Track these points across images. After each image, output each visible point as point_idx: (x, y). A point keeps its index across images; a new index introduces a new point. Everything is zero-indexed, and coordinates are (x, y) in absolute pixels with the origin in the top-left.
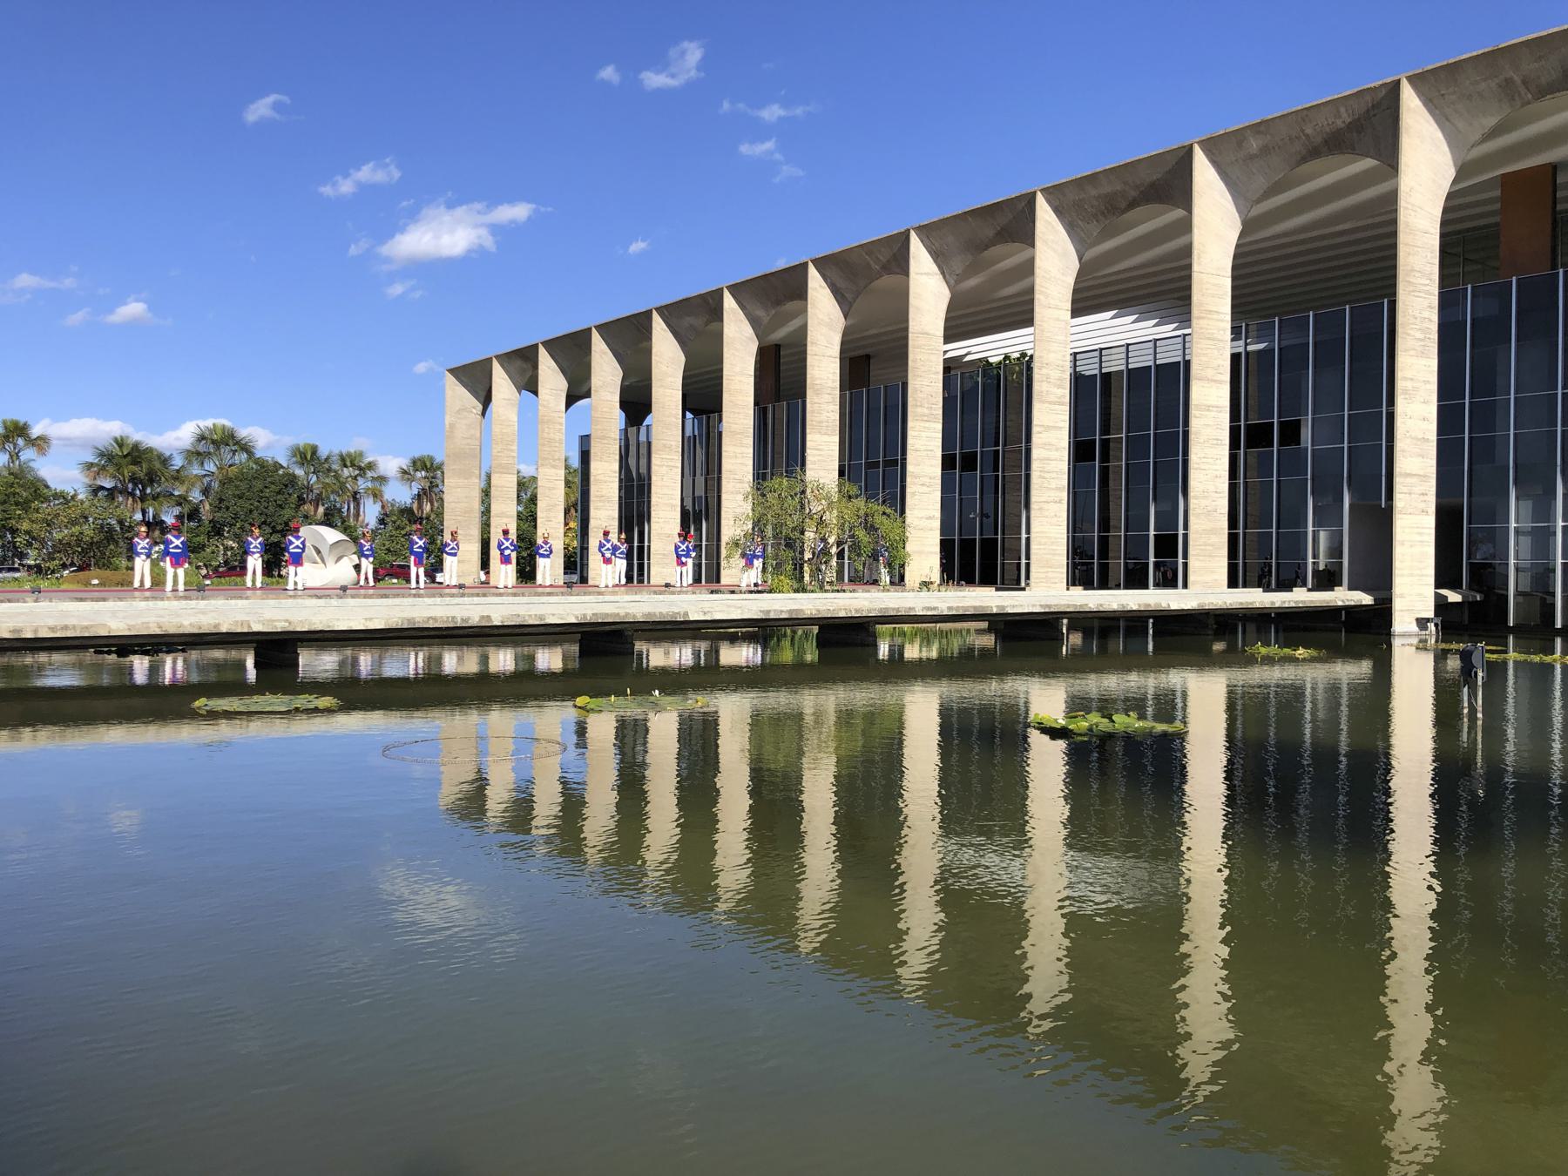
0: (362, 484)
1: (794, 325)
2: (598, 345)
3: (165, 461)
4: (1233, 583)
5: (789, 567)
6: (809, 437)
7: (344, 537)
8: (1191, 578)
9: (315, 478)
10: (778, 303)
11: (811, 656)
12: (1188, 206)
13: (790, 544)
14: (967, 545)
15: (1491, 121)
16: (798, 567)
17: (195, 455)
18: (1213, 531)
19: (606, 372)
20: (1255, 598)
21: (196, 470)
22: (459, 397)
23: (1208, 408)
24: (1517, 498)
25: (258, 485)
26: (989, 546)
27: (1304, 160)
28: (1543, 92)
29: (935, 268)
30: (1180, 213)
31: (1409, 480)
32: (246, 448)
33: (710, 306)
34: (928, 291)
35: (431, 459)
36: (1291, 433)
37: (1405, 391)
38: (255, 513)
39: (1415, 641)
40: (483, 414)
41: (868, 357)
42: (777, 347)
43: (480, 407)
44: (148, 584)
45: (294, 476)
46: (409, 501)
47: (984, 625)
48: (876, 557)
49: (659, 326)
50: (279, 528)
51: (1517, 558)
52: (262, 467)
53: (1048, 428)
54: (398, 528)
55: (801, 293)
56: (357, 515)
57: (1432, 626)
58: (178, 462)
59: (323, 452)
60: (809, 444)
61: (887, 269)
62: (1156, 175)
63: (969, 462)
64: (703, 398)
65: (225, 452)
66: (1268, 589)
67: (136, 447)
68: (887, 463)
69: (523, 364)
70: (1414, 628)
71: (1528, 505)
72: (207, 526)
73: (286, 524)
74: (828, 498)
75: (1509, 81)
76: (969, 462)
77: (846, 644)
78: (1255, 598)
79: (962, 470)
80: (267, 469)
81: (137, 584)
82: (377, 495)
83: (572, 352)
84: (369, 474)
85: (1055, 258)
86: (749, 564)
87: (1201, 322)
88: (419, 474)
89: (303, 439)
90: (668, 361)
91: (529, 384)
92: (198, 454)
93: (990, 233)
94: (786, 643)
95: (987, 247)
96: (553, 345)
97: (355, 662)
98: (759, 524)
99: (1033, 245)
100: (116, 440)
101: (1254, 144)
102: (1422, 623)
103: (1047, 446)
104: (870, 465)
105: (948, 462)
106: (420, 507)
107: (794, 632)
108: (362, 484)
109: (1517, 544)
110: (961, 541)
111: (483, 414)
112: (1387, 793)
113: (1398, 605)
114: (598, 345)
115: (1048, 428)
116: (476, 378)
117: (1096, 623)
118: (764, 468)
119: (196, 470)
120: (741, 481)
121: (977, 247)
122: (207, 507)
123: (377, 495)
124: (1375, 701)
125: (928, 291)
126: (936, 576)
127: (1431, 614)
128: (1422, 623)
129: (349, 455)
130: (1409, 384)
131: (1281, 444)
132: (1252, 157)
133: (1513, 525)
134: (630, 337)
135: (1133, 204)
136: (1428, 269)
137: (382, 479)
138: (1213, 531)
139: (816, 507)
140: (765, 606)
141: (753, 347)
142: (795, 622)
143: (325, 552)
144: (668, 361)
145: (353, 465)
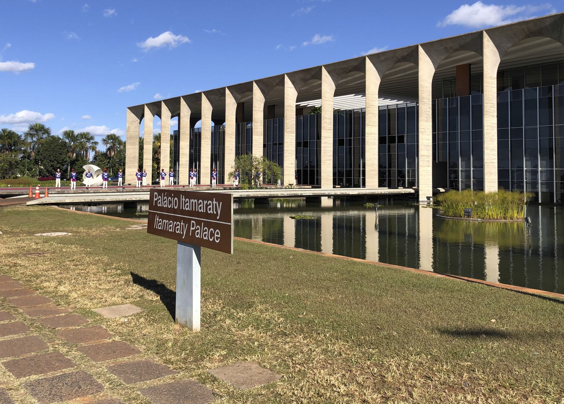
0: (88, 145)
1: (249, 97)
2: (183, 103)
3: (19, 137)
4: (380, 185)
5: (247, 181)
6: (253, 137)
7: (99, 168)
8: (367, 184)
9: (72, 143)
10: (243, 93)
11: (253, 206)
12: (365, 72)
13: (247, 174)
14: (305, 172)
15: (443, 57)
16: (250, 183)
17: (27, 134)
18: (373, 170)
19: (185, 111)
20: (385, 190)
21: (29, 140)
22: (132, 117)
23: (371, 134)
24: (461, 161)
25: (53, 146)
26: (312, 172)
27: (397, 62)
28: (456, 50)
29: (293, 86)
30: (363, 74)
31: (423, 157)
32: (47, 131)
33: (279, 81)
34: (290, 93)
35: (114, 135)
36: (401, 139)
37: (422, 132)
38: (52, 157)
39: (426, 203)
40: (140, 123)
41: (274, 106)
42: (243, 103)
43: (139, 121)
44: (59, 186)
45: (66, 142)
46: (105, 151)
47: (305, 198)
48: (273, 179)
49: (204, 97)
50: (60, 162)
51: (461, 178)
52: (54, 139)
53: (326, 137)
54: (101, 161)
55: (251, 90)
56: (87, 156)
57: (431, 199)
58: (23, 138)
59: (76, 133)
60: (253, 139)
61: (278, 84)
62: (356, 64)
63: (306, 145)
64: (219, 118)
65: (40, 133)
66: (404, 187)
67: (10, 132)
68: (280, 144)
69: (156, 108)
70: (426, 199)
71: (464, 163)
72: (33, 161)
73: (63, 160)
74: (258, 161)
75: (446, 48)
76: (306, 145)
77: (262, 204)
78: (385, 190)
79: (304, 147)
80: (55, 139)
81: (57, 186)
82: (94, 149)
83: (174, 105)
84: (92, 141)
85: (328, 84)
86: (236, 179)
87: (369, 109)
88: (110, 141)
89: (67, 129)
90: (207, 108)
91: (157, 113)
92: (31, 134)
93: (309, 77)
94: (246, 203)
95: (308, 80)
96: (167, 102)
97: (117, 208)
98: (237, 168)
99: (321, 80)
100: (3, 130)
101: (383, 58)
102: (428, 198)
103: (326, 143)
104: (274, 144)
105: (298, 144)
106: (110, 153)
107: (248, 200)
108: (88, 145)
109: (461, 174)
110: (398, 137)
111: (140, 123)
112: (418, 245)
113: (421, 193)
114: (183, 103)
115: (326, 137)
116: (139, 112)
117: (345, 198)
118: (238, 153)
119: (29, 140)
120: (231, 150)
121: (305, 80)
122: (33, 154)
123: (94, 149)
124: (415, 219)
125: (290, 93)
126: (295, 183)
127: (431, 196)
128: (428, 198)
129: (84, 134)
130: (423, 130)
131: (398, 142)
132: (382, 61)
133: (460, 169)
134: (194, 101)
135: (351, 71)
136: (428, 97)
137: (96, 143)
138: (373, 170)
139: (254, 163)
140: (241, 194)
141: (236, 106)
142: (248, 198)
143: (93, 174)
144: (207, 108)
145: (85, 138)
